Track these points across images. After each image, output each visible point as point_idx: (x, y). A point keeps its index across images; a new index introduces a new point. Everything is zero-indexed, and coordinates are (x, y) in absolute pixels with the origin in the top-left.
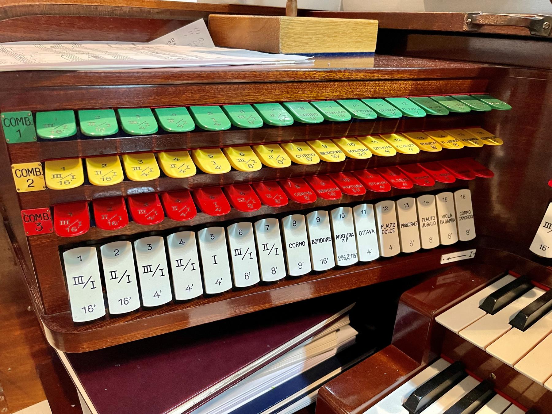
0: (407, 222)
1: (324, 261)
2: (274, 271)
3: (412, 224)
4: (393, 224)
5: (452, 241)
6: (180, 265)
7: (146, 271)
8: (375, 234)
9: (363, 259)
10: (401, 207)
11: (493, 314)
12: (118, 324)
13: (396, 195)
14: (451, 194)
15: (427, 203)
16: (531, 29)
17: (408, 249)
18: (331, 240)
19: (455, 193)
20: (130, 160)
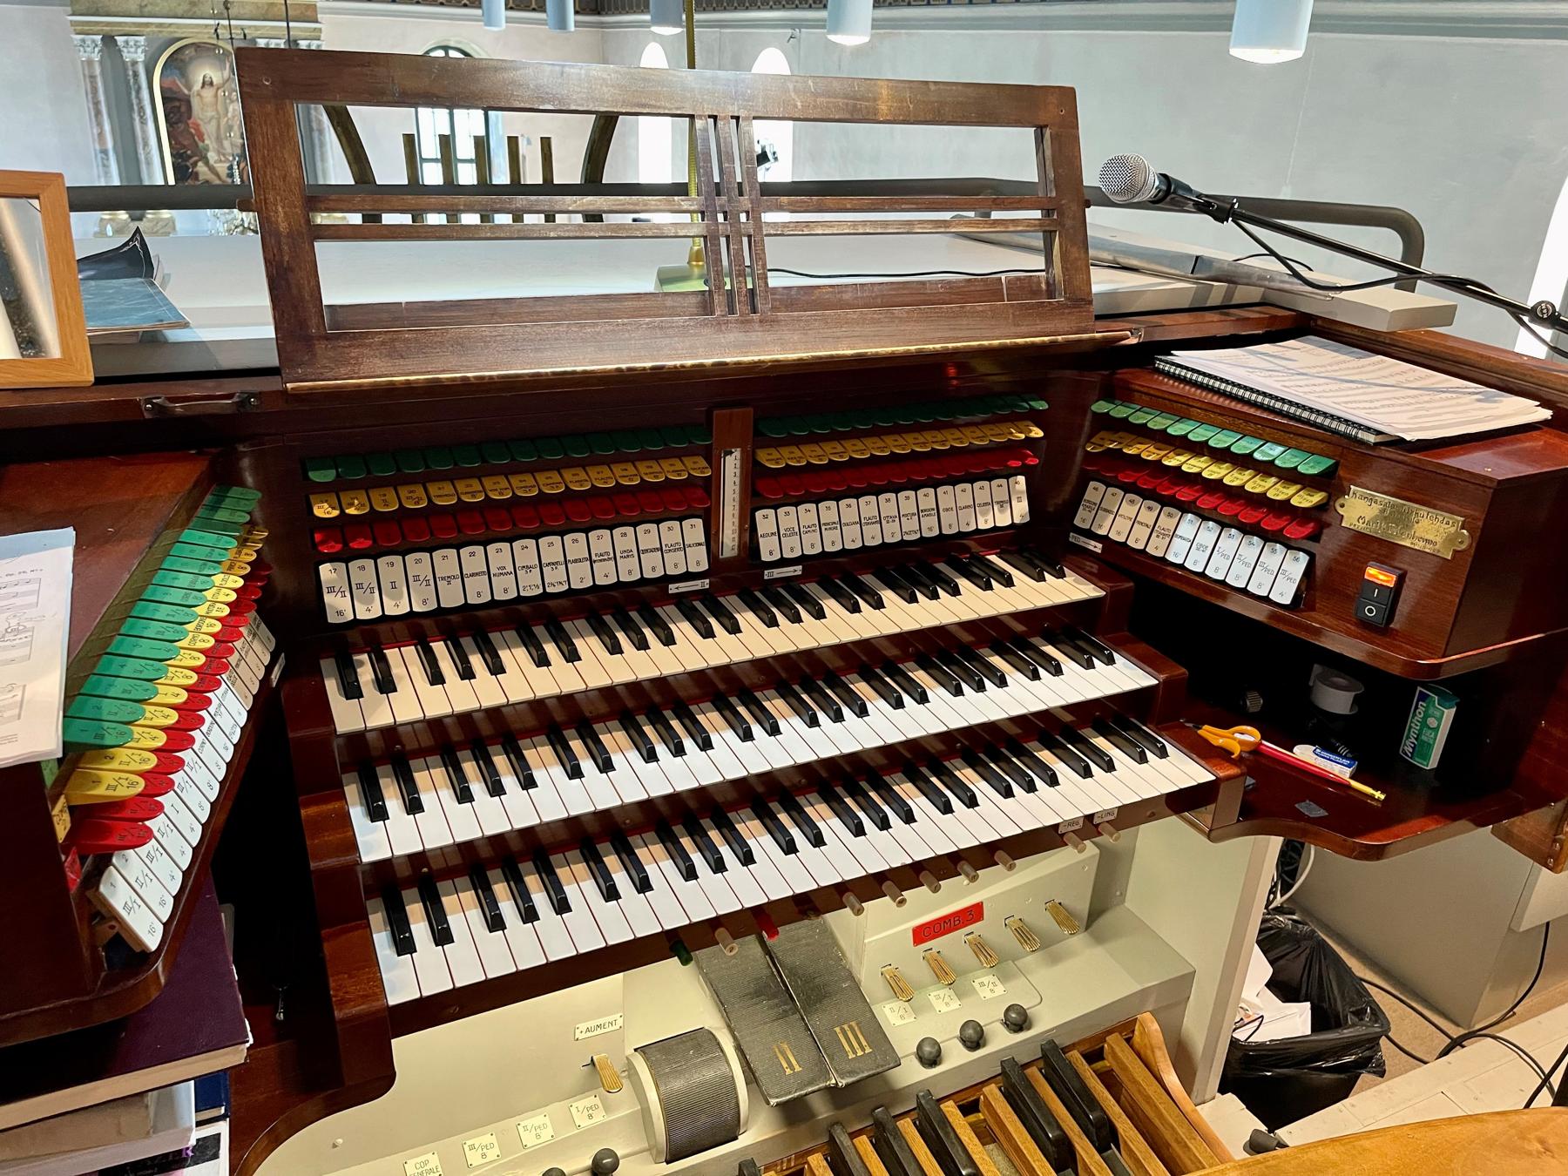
3: (646, 551)
5: (682, 570)
15: (1132, 502)
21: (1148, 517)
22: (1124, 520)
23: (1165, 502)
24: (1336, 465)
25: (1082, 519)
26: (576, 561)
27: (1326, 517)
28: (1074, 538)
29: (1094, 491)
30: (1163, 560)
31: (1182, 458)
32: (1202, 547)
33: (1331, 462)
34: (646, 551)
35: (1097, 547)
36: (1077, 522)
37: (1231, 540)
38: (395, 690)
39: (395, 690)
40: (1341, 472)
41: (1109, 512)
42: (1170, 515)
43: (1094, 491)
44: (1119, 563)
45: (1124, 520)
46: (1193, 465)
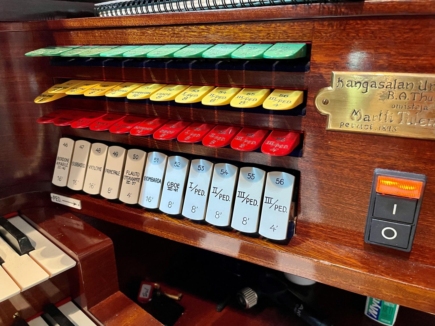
0: (111, 169)
1: (92, 186)
2: (193, 208)
3: (110, 171)
4: (67, 160)
6: (215, 189)
7: (243, 193)
8: (160, 184)
9: (85, 190)
10: (218, 173)
11: (20, 255)
12: (131, 212)
13: (147, 145)
14: (73, 141)
15: (99, 151)
16: (434, 4)
17: (124, 199)
18: (120, 174)
19: (77, 142)
20: (301, 95)
21: (115, 163)
22: (90, 170)
23: (128, 144)
24: (308, 48)
25: (59, 178)
26: (116, 173)
27: (304, 125)
28: (56, 198)
29: (65, 147)
30: (137, 207)
31: (128, 89)
32: (172, 186)
33: (301, 46)
34: (110, 171)
35: (75, 204)
36: (56, 181)
37: (202, 175)
38: (4, 262)
39: (4, 262)
40: (317, 57)
41: (79, 165)
42: (135, 157)
43: (65, 147)
44: (103, 214)
45: (90, 170)
46: (135, 92)
